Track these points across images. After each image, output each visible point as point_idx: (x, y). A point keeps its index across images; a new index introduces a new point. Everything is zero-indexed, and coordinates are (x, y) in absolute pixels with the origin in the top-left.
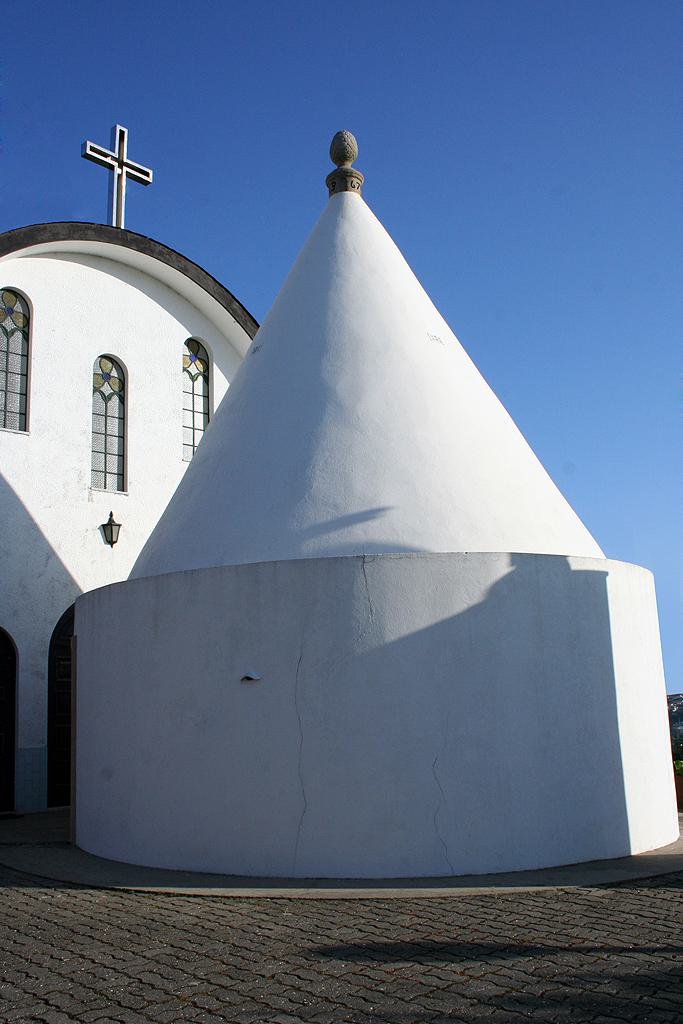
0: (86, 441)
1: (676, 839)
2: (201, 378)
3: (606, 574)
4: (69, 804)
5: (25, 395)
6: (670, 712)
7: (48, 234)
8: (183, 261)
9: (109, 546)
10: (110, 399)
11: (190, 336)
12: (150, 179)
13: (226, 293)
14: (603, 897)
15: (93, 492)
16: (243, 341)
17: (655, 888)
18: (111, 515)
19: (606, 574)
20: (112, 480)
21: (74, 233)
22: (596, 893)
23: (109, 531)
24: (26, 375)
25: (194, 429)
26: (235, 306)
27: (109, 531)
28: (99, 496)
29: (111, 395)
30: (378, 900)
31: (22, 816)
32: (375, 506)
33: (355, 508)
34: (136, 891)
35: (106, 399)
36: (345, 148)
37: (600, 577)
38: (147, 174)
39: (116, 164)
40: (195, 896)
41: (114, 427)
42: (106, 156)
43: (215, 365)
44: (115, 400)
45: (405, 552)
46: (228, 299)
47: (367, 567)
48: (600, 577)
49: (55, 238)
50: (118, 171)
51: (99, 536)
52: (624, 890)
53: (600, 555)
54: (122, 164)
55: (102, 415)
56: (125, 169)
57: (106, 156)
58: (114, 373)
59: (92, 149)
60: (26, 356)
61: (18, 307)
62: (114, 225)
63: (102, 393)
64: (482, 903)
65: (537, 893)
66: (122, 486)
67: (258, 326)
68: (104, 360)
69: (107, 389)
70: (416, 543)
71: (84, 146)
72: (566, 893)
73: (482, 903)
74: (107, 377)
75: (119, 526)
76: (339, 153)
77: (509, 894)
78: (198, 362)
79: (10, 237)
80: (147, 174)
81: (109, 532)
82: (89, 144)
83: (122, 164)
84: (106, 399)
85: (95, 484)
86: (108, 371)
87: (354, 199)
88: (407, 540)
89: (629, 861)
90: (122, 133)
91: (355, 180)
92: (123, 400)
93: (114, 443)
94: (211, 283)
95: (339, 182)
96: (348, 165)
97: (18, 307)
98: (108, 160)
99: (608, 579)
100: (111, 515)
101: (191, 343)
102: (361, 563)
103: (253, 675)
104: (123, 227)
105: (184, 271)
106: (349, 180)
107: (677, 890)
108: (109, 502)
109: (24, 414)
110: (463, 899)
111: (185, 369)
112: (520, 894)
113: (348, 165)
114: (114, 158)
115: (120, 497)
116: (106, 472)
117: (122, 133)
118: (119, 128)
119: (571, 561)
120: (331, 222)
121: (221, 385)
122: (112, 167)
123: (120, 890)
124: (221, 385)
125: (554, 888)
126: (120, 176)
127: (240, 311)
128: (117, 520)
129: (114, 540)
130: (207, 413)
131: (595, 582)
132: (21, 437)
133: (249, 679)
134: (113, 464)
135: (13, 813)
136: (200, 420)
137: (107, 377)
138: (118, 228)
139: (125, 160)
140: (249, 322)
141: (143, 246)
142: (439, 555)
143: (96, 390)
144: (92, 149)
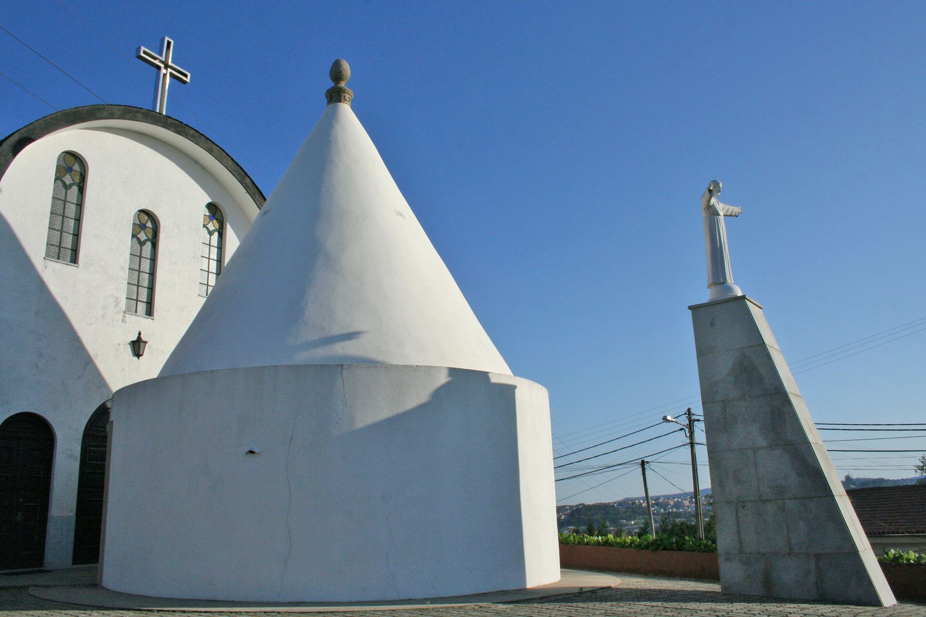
0: (123, 275)
1: (558, 581)
2: (216, 234)
3: (515, 387)
4: (97, 562)
5: (77, 235)
6: (559, 519)
7: (105, 113)
8: (209, 143)
9: (136, 358)
10: (144, 244)
11: (210, 200)
12: (188, 80)
13: (241, 170)
14: (506, 609)
15: (126, 315)
16: (252, 209)
17: (542, 603)
18: (140, 334)
19: (515, 387)
20: (142, 307)
21: (126, 114)
22: (501, 607)
23: (137, 347)
24: (79, 220)
25: (208, 272)
26: (247, 180)
27: (137, 347)
28: (131, 318)
29: (145, 242)
30: (344, 612)
31: (50, 571)
32: (351, 330)
33: (336, 331)
34: (158, 611)
35: (142, 244)
36: (341, 72)
37: (512, 388)
38: (186, 76)
39: (162, 66)
40: (205, 612)
41: (146, 265)
42: (155, 58)
43: (228, 224)
44: (149, 245)
45: (372, 364)
46: (242, 175)
47: (345, 373)
48: (512, 388)
49: (111, 116)
50: (164, 71)
51: (129, 350)
52: (521, 605)
53: (509, 373)
54: (167, 66)
55: (136, 256)
56: (169, 70)
57: (155, 58)
58: (149, 224)
59: (145, 53)
60: (80, 205)
61: (76, 167)
62: (158, 111)
63: (139, 239)
64: (421, 613)
65: (460, 608)
66: (150, 312)
67: (265, 200)
68: (142, 214)
69: (142, 236)
70: (381, 358)
71: (139, 49)
72: (481, 607)
73: (421, 613)
74: (143, 227)
75: (146, 342)
76: (337, 74)
77: (440, 608)
78: (215, 221)
79: (75, 112)
80: (186, 76)
81: (137, 347)
82: (143, 49)
83: (167, 66)
84: (142, 244)
85: (128, 310)
86: (144, 222)
87: (346, 110)
88: (373, 355)
89: (524, 590)
90: (169, 43)
91: (347, 96)
92: (155, 246)
93: (145, 278)
94: (231, 163)
95: (335, 96)
96: (343, 84)
97: (76, 167)
98: (157, 62)
99: (517, 392)
100: (140, 334)
101: (211, 206)
102: (340, 370)
103: (255, 450)
104: (164, 114)
105: (210, 151)
106: (343, 94)
107: (557, 604)
108: (139, 324)
109: (75, 251)
110: (406, 611)
111: (205, 226)
112: (447, 607)
113: (343, 84)
114: (161, 61)
115: (148, 321)
116: (137, 300)
117: (169, 43)
118: (167, 39)
119: (490, 375)
120: (330, 122)
121: (233, 243)
122: (159, 68)
123: (145, 610)
124: (233, 243)
125: (472, 605)
126: (165, 75)
127: (250, 184)
128: (144, 338)
129: (141, 353)
130: (220, 261)
131: (508, 392)
132: (71, 269)
133: (252, 452)
134: (144, 295)
135: (42, 569)
136: (213, 266)
137: (143, 227)
138: (160, 114)
139: (170, 63)
140: (258, 195)
141: (179, 129)
142: (396, 366)
143: (134, 236)
144: (145, 53)
